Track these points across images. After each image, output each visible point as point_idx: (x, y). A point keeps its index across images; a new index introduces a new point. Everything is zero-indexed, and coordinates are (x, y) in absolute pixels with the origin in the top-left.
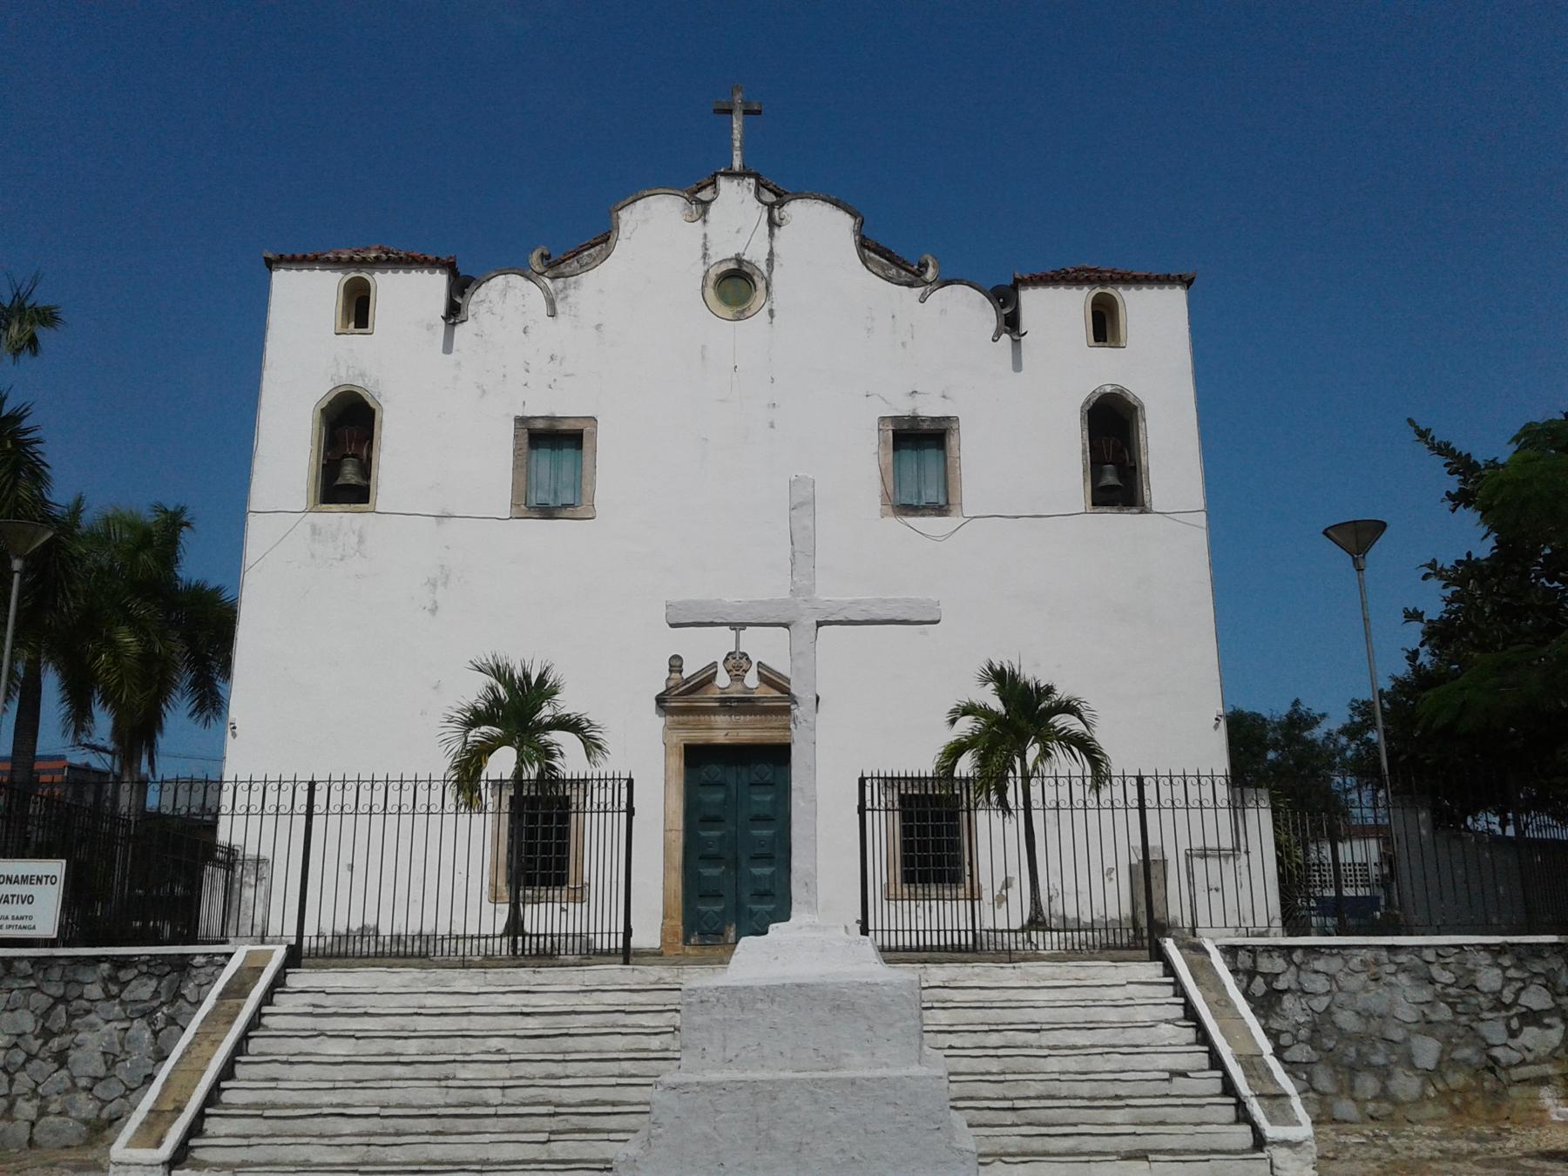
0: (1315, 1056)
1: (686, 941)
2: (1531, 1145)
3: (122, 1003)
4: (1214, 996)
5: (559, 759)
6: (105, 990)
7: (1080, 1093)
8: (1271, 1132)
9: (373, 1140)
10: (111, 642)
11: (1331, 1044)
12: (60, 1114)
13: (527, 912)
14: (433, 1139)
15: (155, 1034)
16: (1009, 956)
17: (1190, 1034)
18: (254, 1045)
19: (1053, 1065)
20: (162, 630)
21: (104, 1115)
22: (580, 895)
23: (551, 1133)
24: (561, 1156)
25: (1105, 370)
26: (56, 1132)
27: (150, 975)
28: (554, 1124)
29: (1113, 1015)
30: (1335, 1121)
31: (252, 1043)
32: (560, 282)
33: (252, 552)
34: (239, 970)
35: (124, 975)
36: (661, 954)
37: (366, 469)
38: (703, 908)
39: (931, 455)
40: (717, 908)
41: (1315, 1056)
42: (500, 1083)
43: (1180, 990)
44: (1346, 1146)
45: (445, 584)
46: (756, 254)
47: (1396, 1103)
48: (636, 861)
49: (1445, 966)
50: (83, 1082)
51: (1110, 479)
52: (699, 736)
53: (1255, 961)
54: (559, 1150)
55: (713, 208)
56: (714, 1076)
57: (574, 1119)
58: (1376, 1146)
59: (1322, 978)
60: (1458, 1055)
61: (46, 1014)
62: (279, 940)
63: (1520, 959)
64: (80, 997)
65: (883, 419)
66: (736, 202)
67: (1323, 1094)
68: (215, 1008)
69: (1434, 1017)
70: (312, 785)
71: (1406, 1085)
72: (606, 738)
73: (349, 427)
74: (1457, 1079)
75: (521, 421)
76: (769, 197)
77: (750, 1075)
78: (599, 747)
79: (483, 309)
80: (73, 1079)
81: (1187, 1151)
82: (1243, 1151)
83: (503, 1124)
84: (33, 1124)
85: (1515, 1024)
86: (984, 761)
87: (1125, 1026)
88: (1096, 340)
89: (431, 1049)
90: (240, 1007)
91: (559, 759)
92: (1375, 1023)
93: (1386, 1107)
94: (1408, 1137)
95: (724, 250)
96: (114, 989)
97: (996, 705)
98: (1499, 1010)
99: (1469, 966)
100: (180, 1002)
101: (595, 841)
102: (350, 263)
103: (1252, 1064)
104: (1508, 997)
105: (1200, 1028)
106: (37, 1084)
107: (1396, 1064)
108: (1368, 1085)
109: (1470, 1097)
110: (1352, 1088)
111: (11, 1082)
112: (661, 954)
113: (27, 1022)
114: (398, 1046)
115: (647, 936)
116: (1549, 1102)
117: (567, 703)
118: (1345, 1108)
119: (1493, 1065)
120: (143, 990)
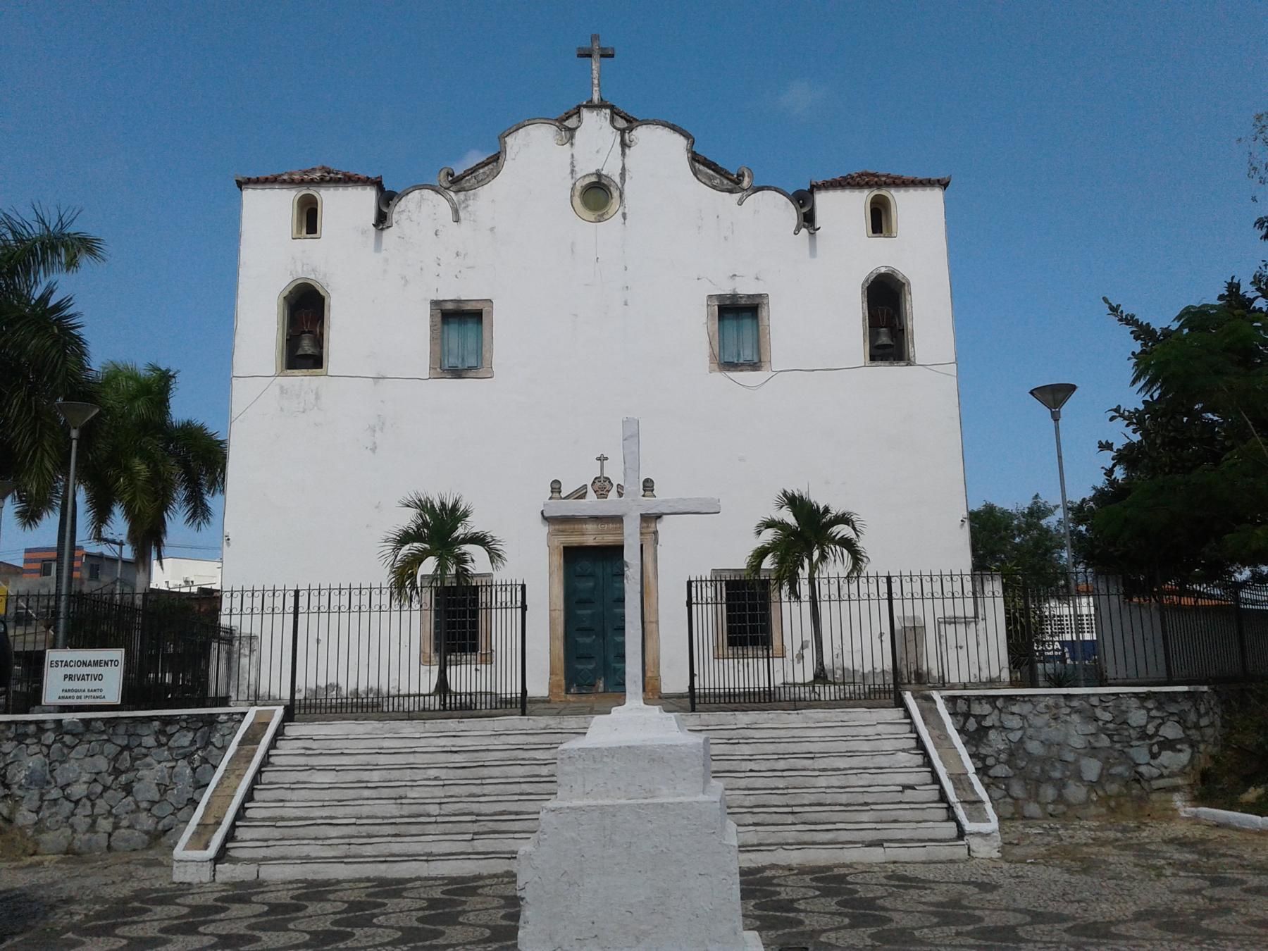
0: (1011, 773)
1: (567, 691)
2: (1170, 834)
3: (170, 748)
4: (937, 732)
5: (471, 564)
6: (157, 740)
7: (840, 801)
8: (969, 826)
9: (353, 841)
10: (128, 470)
11: (1023, 764)
12: (128, 827)
13: (452, 672)
14: (393, 839)
15: (194, 770)
16: (796, 704)
17: (919, 759)
18: (266, 777)
19: (822, 782)
20: (160, 459)
21: (160, 827)
22: (488, 659)
23: (475, 834)
24: (481, 850)
25: (880, 255)
26: (127, 840)
27: (188, 729)
28: (475, 828)
29: (866, 746)
30: (1024, 817)
31: (264, 775)
32: (462, 195)
33: (236, 408)
34: (252, 724)
35: (170, 729)
36: (549, 702)
37: (319, 342)
38: (580, 667)
39: (747, 323)
40: (591, 667)
41: (1011, 773)
42: (438, 801)
43: (914, 730)
44: (1028, 835)
45: (382, 429)
46: (612, 170)
47: (1069, 805)
48: (527, 643)
49: (1105, 709)
50: (144, 805)
51: (884, 339)
52: (575, 540)
53: (969, 707)
54: (479, 845)
55: (578, 133)
56: (576, 803)
57: (490, 824)
58: (1049, 835)
59: (1018, 718)
60: (1113, 771)
61: (116, 759)
62: (277, 701)
63: (1160, 704)
64: (140, 745)
65: (710, 296)
66: (596, 130)
67: (1016, 799)
68: (238, 751)
69: (1097, 745)
70: (297, 593)
71: (1075, 792)
72: (504, 549)
73: (305, 311)
74: (1113, 788)
75: (435, 304)
76: (621, 123)
77: (600, 802)
78: (499, 556)
79: (404, 216)
80: (136, 803)
81: (912, 840)
82: (951, 840)
83: (441, 828)
84: (110, 835)
85: (1155, 749)
86: (781, 562)
87: (875, 753)
88: (874, 232)
89: (389, 777)
90: (255, 751)
91: (471, 564)
92: (1055, 749)
93: (1062, 808)
94: (1073, 829)
95: (587, 167)
96: (163, 740)
97: (791, 520)
98: (1144, 739)
99: (1123, 708)
100: (211, 747)
101: (499, 627)
102: (302, 182)
103: (960, 780)
104: (1151, 730)
105: (926, 754)
106: (112, 807)
107: (1069, 778)
108: (1049, 792)
109: (1122, 800)
110: (1037, 795)
111: (93, 806)
112: (549, 702)
113: (102, 763)
114: (365, 776)
115: (538, 687)
116: (1179, 804)
117: (474, 525)
118: (1033, 809)
119: (1139, 778)
120: (184, 739)
